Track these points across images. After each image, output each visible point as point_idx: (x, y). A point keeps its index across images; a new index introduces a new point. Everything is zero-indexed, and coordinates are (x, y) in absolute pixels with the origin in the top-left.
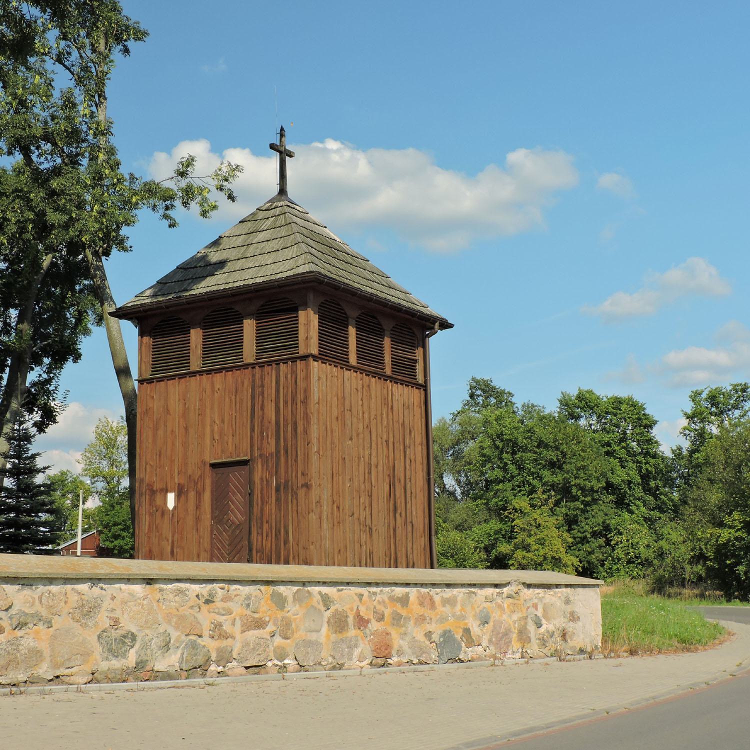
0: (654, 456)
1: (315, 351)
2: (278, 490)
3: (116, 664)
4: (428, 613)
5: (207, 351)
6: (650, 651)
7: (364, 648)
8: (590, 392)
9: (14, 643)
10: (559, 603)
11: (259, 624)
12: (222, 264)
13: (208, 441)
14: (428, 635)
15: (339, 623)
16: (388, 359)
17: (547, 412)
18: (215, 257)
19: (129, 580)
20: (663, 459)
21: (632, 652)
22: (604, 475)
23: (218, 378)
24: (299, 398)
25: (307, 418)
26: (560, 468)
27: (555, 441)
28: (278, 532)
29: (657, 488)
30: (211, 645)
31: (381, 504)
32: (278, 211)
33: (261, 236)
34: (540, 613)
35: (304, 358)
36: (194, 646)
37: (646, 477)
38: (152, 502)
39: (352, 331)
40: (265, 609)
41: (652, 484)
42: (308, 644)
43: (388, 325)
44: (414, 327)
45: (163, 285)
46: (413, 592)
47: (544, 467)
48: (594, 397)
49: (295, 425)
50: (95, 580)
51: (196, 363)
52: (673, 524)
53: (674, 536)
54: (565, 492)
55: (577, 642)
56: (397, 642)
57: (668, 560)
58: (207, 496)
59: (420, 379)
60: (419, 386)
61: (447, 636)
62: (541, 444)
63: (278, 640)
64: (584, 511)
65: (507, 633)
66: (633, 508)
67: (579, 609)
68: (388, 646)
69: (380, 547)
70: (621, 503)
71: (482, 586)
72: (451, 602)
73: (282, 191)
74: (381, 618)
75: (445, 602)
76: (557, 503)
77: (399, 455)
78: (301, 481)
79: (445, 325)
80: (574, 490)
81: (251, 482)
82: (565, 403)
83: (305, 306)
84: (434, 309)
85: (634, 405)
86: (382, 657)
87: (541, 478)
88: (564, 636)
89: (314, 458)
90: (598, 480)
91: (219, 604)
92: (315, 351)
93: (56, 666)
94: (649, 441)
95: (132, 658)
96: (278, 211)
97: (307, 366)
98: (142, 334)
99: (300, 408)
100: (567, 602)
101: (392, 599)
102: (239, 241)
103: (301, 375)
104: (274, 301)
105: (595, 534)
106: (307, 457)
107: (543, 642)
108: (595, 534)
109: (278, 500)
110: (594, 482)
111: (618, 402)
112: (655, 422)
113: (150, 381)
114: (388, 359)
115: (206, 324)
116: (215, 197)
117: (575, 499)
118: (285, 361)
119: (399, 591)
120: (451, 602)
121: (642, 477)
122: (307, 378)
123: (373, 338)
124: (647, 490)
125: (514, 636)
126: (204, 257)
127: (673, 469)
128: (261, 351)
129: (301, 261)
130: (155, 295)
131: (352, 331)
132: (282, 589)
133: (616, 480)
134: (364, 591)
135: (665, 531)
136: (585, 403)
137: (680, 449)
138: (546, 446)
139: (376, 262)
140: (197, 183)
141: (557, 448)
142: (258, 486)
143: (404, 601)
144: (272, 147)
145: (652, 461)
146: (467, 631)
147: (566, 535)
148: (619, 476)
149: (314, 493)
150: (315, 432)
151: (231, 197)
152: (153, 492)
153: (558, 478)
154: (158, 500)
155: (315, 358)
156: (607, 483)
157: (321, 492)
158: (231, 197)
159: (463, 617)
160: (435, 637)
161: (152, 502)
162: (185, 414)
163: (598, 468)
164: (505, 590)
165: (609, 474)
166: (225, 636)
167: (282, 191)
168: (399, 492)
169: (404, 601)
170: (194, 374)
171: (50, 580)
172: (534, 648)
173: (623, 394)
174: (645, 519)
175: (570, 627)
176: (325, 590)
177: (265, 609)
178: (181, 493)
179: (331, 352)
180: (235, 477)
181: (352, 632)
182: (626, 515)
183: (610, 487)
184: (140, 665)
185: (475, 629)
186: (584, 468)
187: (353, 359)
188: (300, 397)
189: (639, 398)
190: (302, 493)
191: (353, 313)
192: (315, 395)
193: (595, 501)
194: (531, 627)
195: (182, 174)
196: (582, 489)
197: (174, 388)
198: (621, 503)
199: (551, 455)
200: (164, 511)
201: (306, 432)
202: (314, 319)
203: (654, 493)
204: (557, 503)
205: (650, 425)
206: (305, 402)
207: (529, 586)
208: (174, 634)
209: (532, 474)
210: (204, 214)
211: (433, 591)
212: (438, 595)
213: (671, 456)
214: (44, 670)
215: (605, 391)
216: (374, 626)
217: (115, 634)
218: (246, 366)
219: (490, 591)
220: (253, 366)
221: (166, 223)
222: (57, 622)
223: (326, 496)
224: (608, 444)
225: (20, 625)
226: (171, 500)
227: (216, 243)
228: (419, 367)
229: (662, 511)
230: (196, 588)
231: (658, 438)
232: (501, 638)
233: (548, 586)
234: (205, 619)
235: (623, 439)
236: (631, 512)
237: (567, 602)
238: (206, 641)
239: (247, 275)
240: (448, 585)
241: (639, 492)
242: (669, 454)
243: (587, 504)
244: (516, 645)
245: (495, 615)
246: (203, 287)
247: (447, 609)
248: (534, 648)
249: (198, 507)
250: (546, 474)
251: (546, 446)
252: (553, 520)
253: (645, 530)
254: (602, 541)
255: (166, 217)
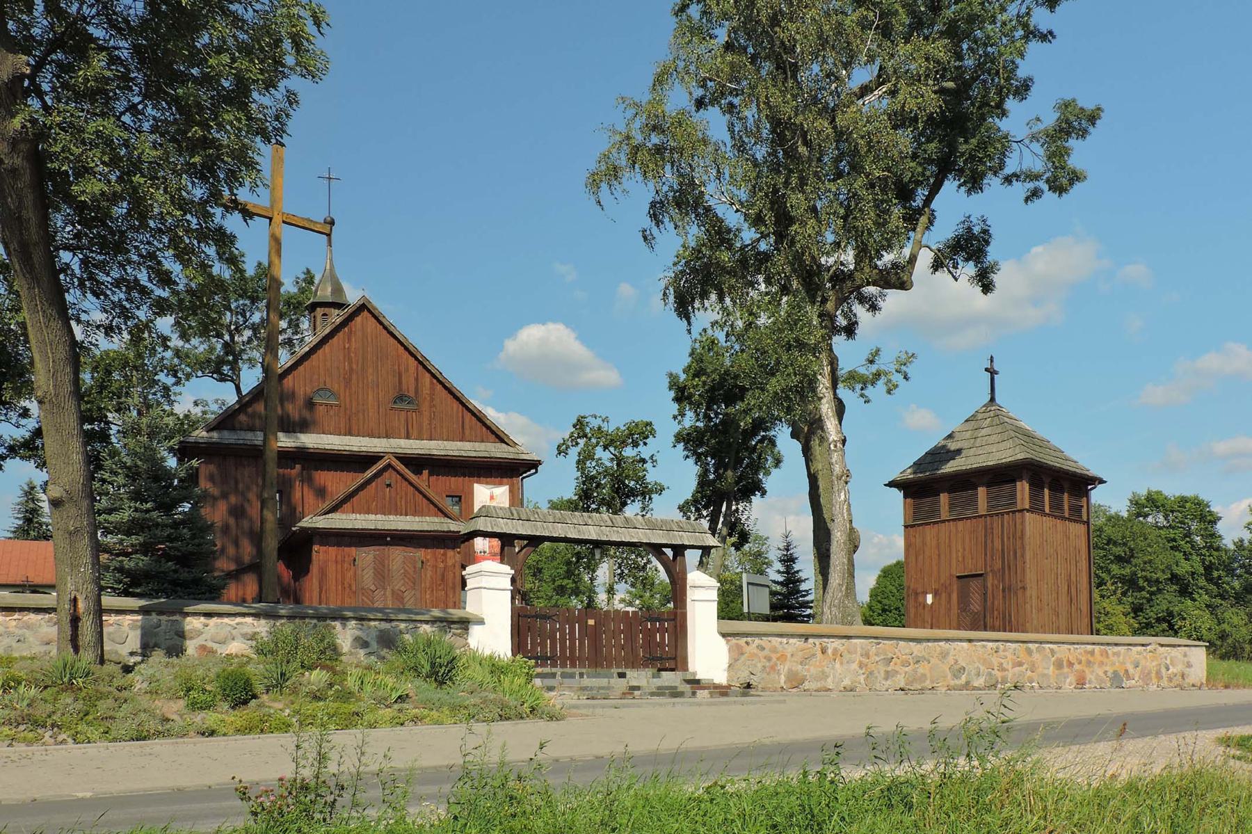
0: (1218, 549)
1: (1027, 507)
2: (1004, 591)
3: (957, 682)
4: (1105, 660)
5: (952, 506)
6: (1237, 686)
7: (1071, 679)
8: (1159, 493)
9: (915, 671)
10: (1180, 656)
11: (1020, 664)
12: (959, 452)
13: (954, 562)
14: (1105, 672)
15: (1059, 664)
16: (1066, 507)
17: (1113, 512)
18: (953, 446)
19: (961, 640)
20: (1226, 551)
21: (1226, 687)
22: (1169, 567)
23: (960, 524)
24: (1018, 535)
25: (1023, 547)
26: (1128, 562)
27: (1124, 537)
28: (1004, 618)
29: (1220, 577)
30: (999, 674)
31: (1064, 598)
32: (992, 414)
33: (984, 432)
34: (1168, 662)
35: (1021, 511)
36: (990, 674)
37: (1208, 569)
38: (916, 600)
39: (1046, 491)
40: (1023, 656)
41: (1215, 574)
42: (1044, 675)
43: (1066, 485)
44: (1081, 484)
45: (918, 465)
46: (1097, 648)
47: (1112, 562)
48: (1161, 498)
49: (1015, 553)
50: (947, 640)
51: (945, 514)
52: (1234, 610)
53: (1235, 620)
54: (1131, 583)
55: (1192, 679)
56: (1089, 676)
57: (1230, 641)
58: (954, 596)
59: (1085, 518)
60: (1084, 523)
61: (1115, 673)
62: (1109, 541)
63: (1029, 673)
64: (1149, 600)
65: (1149, 673)
66: (1196, 596)
67: (1193, 660)
68: (1084, 678)
69: (1063, 622)
70: (1185, 591)
71: (1135, 645)
72: (1117, 654)
73: (992, 399)
74: (1080, 663)
75: (1114, 654)
76: (1124, 594)
77: (1073, 567)
78: (1020, 585)
79: (1102, 482)
80: (1141, 582)
81: (985, 587)
82: (1135, 503)
83: (1021, 479)
84: (1094, 471)
85: (1198, 503)
86: (1081, 683)
87: (1109, 572)
88: (1183, 676)
89: (1028, 571)
90: (1163, 571)
91: (1001, 653)
92: (1027, 507)
93: (932, 682)
94: (1213, 535)
95: (963, 679)
96: (992, 414)
97: (1023, 517)
98: (905, 497)
99: (1019, 542)
100: (1185, 655)
101: (1087, 652)
102: (968, 435)
103: (1018, 522)
104: (1001, 476)
105: (1158, 620)
106: (1024, 570)
107: (1170, 679)
108: (1158, 620)
109: (1004, 597)
110: (1159, 574)
111: (1183, 501)
112: (1220, 519)
113: (912, 526)
114: (1066, 507)
115: (951, 490)
116: (896, 378)
117: (1143, 589)
118: (1008, 513)
119: (1089, 647)
120: (1117, 654)
121: (1205, 569)
122: (1023, 523)
123: (1058, 495)
124: (1210, 580)
125: (1153, 675)
126: (944, 446)
127: (1235, 560)
128: (990, 507)
129: (1017, 450)
130: (914, 473)
131: (1046, 491)
132: (1030, 645)
133: (1179, 571)
134: (1071, 647)
135: (1227, 615)
136: (1153, 502)
137: (1242, 541)
138: (1115, 544)
139: (1055, 442)
140: (883, 367)
141: (1125, 544)
142: (990, 591)
143: (1092, 653)
144: (987, 370)
145: (1215, 553)
146: (1127, 671)
147: (1132, 621)
148: (1184, 568)
149: (1028, 593)
150: (1028, 555)
151: (906, 378)
152: (917, 594)
153: (1127, 571)
154: (920, 599)
155: (1028, 511)
156: (1172, 574)
157: (1032, 592)
158: (906, 378)
159: (1123, 663)
160: (1109, 674)
161: (916, 600)
162: (938, 546)
163: (1163, 560)
164: (1149, 648)
165: (1174, 567)
166: (1004, 670)
167: (992, 399)
168: (1073, 590)
169: (1092, 653)
170: (944, 521)
171: (928, 640)
172: (1164, 683)
173: (1189, 493)
174: (1207, 606)
175: (1187, 671)
176: (1051, 646)
177: (1023, 656)
178: (936, 594)
179: (1036, 508)
180: (974, 584)
181: (1066, 670)
182: (1189, 602)
183: (1174, 578)
184: (968, 683)
185: (1131, 671)
186: (1150, 561)
187: (1047, 510)
188: (1019, 534)
189: (1204, 497)
190: (1020, 593)
191: (1047, 480)
192: (1028, 533)
193: (1160, 591)
194: (1163, 670)
195: (872, 362)
196: (1146, 579)
197: (930, 532)
198: (1185, 591)
199: (1119, 550)
200: (925, 605)
201: (1023, 556)
202: (1027, 486)
203: (1216, 582)
204: (1124, 594)
205: (1214, 520)
206: (1022, 537)
207: (1162, 646)
208: (982, 668)
209: (1102, 568)
210: (889, 391)
211: (1107, 648)
212: (1111, 650)
213: (1232, 547)
214: (928, 684)
215: (1172, 489)
216: (1077, 667)
217: (957, 667)
218: (981, 516)
219: (1140, 648)
220: (985, 516)
221: (863, 400)
222: (933, 661)
223: (1034, 594)
224: (1174, 540)
225: (918, 662)
226: (929, 599)
227: (950, 436)
228: (1084, 510)
229: (1223, 598)
230: (990, 644)
231: (1221, 533)
232: (1146, 677)
233: (1174, 646)
234: (995, 661)
235: (1188, 535)
236: (1194, 600)
237: (1185, 655)
238: (995, 672)
239: (972, 460)
240: (1116, 645)
241: (1202, 582)
242: (1232, 547)
243: (1152, 593)
244: (1155, 680)
245: (1143, 662)
246: (950, 467)
247: (1115, 659)
248: (1164, 683)
249: (949, 602)
250: (1115, 569)
251: (1115, 544)
252: (1120, 608)
253: (1207, 615)
254: (1165, 625)
255: (862, 395)
